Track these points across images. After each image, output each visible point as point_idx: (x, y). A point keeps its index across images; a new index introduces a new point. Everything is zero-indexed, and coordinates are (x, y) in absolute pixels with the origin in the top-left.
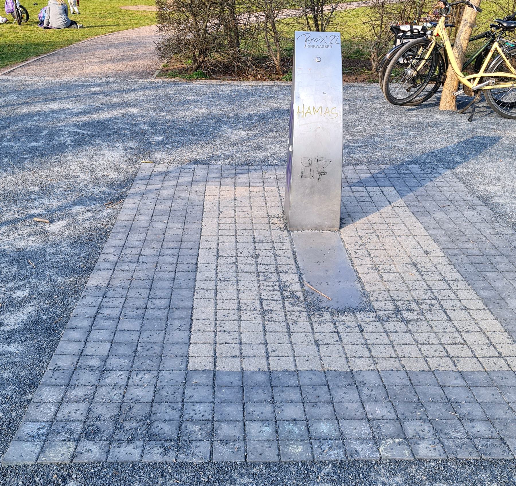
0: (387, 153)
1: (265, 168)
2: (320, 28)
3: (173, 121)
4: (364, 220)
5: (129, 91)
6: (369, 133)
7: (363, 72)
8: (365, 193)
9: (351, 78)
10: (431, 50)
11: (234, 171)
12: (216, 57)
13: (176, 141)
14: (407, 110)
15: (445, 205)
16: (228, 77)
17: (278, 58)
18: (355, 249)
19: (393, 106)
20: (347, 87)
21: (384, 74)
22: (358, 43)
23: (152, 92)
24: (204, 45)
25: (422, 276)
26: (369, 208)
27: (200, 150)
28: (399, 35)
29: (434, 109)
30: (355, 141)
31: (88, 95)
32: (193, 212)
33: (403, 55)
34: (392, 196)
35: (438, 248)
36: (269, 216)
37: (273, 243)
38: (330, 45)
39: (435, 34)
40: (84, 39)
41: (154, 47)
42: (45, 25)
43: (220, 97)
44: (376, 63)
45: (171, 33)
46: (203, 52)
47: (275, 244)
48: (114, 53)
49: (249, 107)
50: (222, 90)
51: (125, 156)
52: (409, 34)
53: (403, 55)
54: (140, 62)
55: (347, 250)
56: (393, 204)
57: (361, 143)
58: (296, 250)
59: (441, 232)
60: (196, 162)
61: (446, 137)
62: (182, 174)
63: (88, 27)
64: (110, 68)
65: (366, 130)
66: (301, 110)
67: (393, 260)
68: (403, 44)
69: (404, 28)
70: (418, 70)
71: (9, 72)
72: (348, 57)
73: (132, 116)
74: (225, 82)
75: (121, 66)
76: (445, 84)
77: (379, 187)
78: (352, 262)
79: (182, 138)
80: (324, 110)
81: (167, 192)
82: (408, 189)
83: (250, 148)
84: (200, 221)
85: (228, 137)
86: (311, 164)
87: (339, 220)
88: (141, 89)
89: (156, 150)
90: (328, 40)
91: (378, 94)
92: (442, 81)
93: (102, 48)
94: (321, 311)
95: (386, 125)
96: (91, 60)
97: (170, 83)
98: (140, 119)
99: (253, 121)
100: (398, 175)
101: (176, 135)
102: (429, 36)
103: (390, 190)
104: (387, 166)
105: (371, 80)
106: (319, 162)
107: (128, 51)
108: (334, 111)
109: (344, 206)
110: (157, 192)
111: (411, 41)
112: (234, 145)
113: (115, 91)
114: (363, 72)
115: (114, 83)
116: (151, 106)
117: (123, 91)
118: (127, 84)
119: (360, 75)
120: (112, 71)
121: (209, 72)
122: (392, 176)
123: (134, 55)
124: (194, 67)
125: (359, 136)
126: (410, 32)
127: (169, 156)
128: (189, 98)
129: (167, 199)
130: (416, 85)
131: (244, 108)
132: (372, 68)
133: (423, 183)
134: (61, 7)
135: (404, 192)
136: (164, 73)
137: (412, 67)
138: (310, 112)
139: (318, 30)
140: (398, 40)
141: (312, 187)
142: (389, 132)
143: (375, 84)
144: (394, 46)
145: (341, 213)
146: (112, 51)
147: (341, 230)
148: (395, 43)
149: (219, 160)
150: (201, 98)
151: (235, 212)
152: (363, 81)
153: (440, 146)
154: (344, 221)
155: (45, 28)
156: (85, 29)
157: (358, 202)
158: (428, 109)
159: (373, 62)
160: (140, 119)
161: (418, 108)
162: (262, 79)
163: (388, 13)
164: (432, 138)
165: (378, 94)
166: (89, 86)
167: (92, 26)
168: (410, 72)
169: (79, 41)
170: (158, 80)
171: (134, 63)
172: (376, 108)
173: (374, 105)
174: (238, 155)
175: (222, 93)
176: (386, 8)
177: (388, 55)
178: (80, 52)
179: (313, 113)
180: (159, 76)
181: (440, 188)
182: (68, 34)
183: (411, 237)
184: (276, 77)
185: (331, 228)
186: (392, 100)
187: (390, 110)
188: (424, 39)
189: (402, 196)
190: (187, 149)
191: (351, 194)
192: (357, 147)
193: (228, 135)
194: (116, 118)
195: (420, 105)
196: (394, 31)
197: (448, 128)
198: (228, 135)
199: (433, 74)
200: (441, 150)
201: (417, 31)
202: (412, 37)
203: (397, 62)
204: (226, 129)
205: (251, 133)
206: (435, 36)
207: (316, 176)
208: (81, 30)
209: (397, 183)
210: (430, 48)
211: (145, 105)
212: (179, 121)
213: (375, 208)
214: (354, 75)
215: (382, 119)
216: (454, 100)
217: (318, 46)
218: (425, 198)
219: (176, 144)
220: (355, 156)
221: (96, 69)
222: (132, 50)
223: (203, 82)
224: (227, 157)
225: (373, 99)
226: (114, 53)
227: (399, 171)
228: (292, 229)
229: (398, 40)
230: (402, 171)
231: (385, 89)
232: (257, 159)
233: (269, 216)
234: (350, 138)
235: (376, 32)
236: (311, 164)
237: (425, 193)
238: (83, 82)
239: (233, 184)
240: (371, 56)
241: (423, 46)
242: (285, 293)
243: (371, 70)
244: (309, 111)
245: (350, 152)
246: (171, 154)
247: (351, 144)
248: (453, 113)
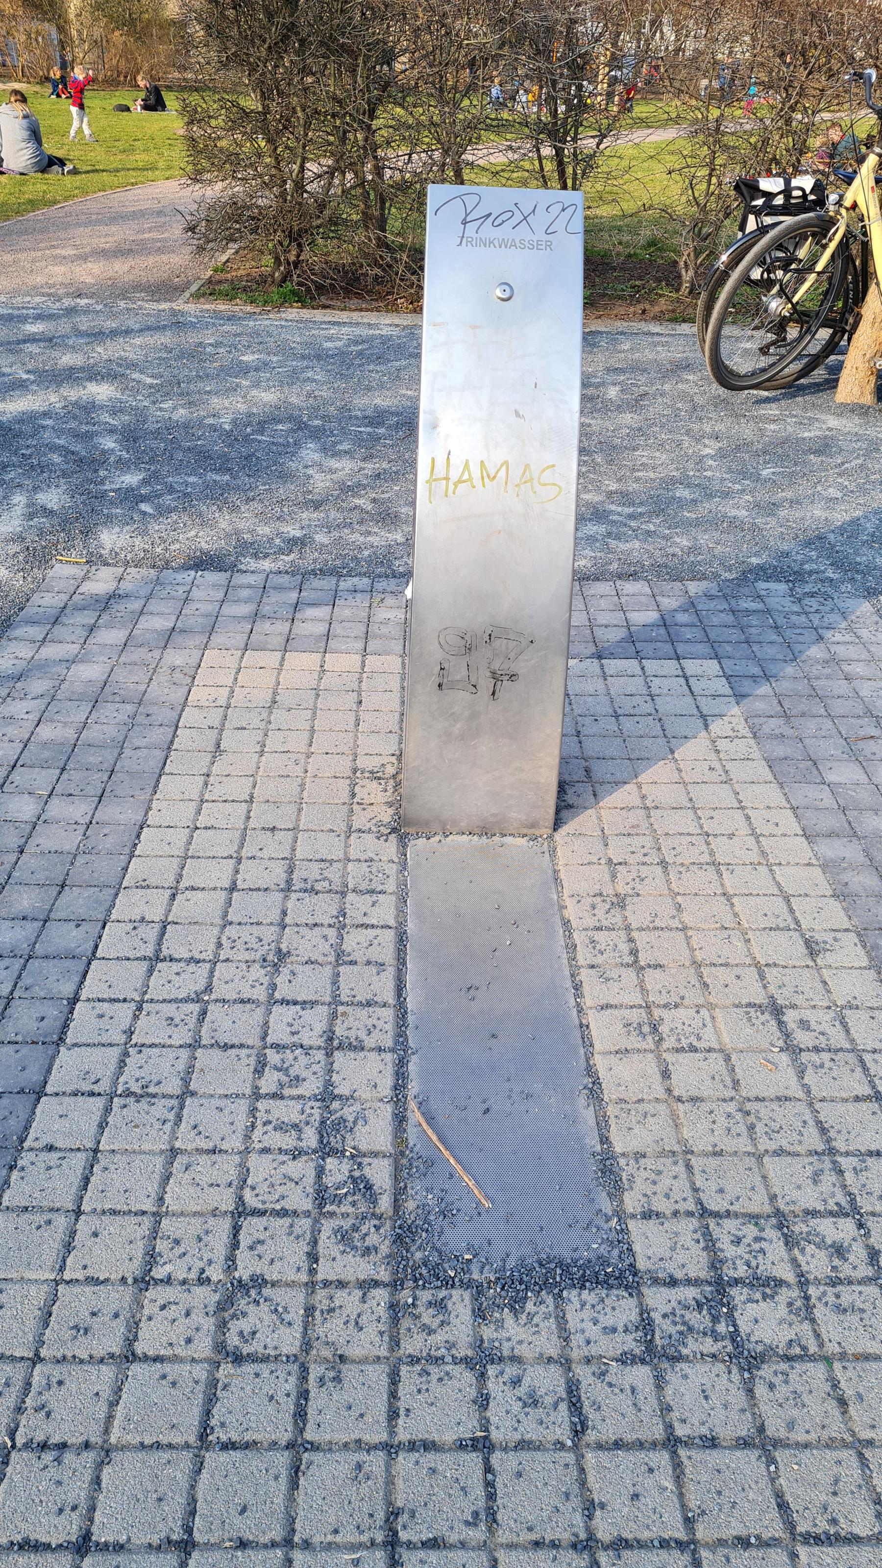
0: (704, 539)
1: (381, 585)
2: (569, 182)
3: (186, 426)
4: (625, 795)
5: (114, 333)
6: (662, 473)
7: (661, 296)
8: (636, 685)
9: (632, 309)
10: (833, 246)
11: (294, 595)
12: (325, 252)
13: (171, 490)
14: (757, 402)
15: (862, 733)
16: (354, 303)
18: (591, 922)
19: (722, 391)
20: (622, 333)
21: (709, 308)
22: (656, 222)
23: (166, 339)
24: (298, 222)
25: (801, 1073)
26: (646, 742)
27: (224, 521)
28: (754, 203)
29: (820, 398)
30: (625, 498)
31: (9, 343)
32: (139, 753)
33: (760, 261)
34: (714, 696)
35: (847, 925)
36: (355, 771)
37: (343, 894)
39: (848, 203)
40: (66, 199)
43: (321, 356)
44: (691, 273)
45: (216, 190)
46: (296, 237)
47: (351, 897)
48: (118, 234)
49: (382, 386)
50: (330, 339)
51: (19, 538)
52: (779, 201)
53: (760, 261)
54: (165, 258)
55: (566, 923)
56: (716, 727)
57: (641, 504)
58: (411, 927)
59: (852, 852)
60: (202, 562)
61: (852, 487)
62: (152, 606)
63: (88, 172)
64: (90, 273)
65: (654, 463)
66: (440, 471)
67: (706, 985)
68: (763, 230)
69: (768, 184)
70: (795, 300)
72: (630, 256)
73: (89, 408)
74: (344, 316)
75: (120, 267)
76: (855, 336)
77: (678, 659)
78: (578, 987)
79: (192, 479)
81: (90, 673)
82: (756, 671)
83: (355, 516)
84: (149, 790)
85: (309, 477)
86: (469, 649)
87: (554, 788)
88: (141, 330)
89: (109, 520)
90: (539, 221)
91: (691, 355)
92: (848, 328)
93: (99, 222)
94: (438, 1276)
95: (705, 446)
96: (58, 251)
97: (216, 314)
98: (105, 417)
99: (382, 431)
100: (729, 619)
101: (177, 471)
102: (832, 208)
103: (705, 670)
104: (704, 584)
105: (678, 318)
106: (497, 643)
107: (150, 230)
108: (547, 477)
109: (574, 733)
110: (61, 669)
111: (788, 220)
112: (317, 505)
113: (79, 333)
114: (661, 296)
115: (86, 311)
116: (149, 381)
117: (98, 336)
118: (114, 316)
119: (653, 303)
120: (93, 281)
121: (308, 290)
122: (715, 620)
123: (159, 240)
124: (277, 274)
125: (637, 480)
126: (781, 196)
127: (138, 541)
128: (245, 358)
129: (80, 698)
130: (785, 339)
131: (369, 389)
132: (680, 284)
133: (797, 648)
134: (25, 122)
136: (212, 289)
137: (782, 292)
138: (470, 479)
139: (564, 187)
140: (751, 218)
141: (474, 716)
142: (714, 471)
143: (685, 328)
144: (740, 235)
145: (564, 761)
146: (114, 228)
147: (559, 836)
148: (742, 227)
149: (266, 556)
150: (275, 359)
151: (262, 753)
152: (658, 318)
153: (840, 517)
154: (570, 798)
156: (79, 177)
157: (617, 716)
158: (807, 398)
159: (683, 272)
160: (105, 417)
161: (785, 396)
163: (726, 148)
164: (819, 488)
165: (691, 355)
166: (23, 319)
167: (96, 171)
168: (776, 305)
169: (55, 202)
170: (191, 307)
171: (151, 260)
172: (683, 396)
173: (680, 386)
174: (321, 538)
175: (329, 345)
176: (724, 134)
177: (724, 258)
178: (43, 230)
179: (477, 482)
180: (197, 296)
181: (846, 668)
182: (38, 185)
183: (763, 869)
185: (529, 831)
186: (725, 376)
187: (717, 403)
188: (818, 217)
189: (740, 697)
190: (190, 516)
191: (600, 685)
192: (631, 517)
193: (310, 471)
194: (46, 415)
195: (792, 388)
196: (742, 194)
197: (858, 457)
198: (310, 471)
199: (831, 309)
200: (842, 530)
201: (800, 193)
202: (786, 210)
203: (746, 280)
204: (310, 453)
205: (370, 467)
206: (847, 209)
207: (486, 684)
208: (68, 179)
209: (728, 648)
210: (830, 240)
211: (136, 375)
212: (201, 425)
213: (662, 741)
214: (639, 302)
215: (696, 427)
216: (873, 379)
217: (504, 244)
218: (803, 707)
219: (168, 500)
220: (623, 546)
221: (59, 273)
222: (158, 228)
223: (293, 313)
224: (293, 543)
225: (680, 367)
226: (118, 234)
228: (412, 830)
229: (751, 218)
231: (711, 350)
232: (366, 553)
233: (355, 771)
234: (614, 487)
235: (697, 195)
236: (469, 649)
237: (802, 687)
238: (13, 308)
239: (280, 641)
240: (680, 255)
241: (814, 235)
242: (337, 1171)
243: (678, 290)
244: (466, 476)
245: (609, 534)
246: (145, 532)
247: (613, 507)
248: (866, 413)
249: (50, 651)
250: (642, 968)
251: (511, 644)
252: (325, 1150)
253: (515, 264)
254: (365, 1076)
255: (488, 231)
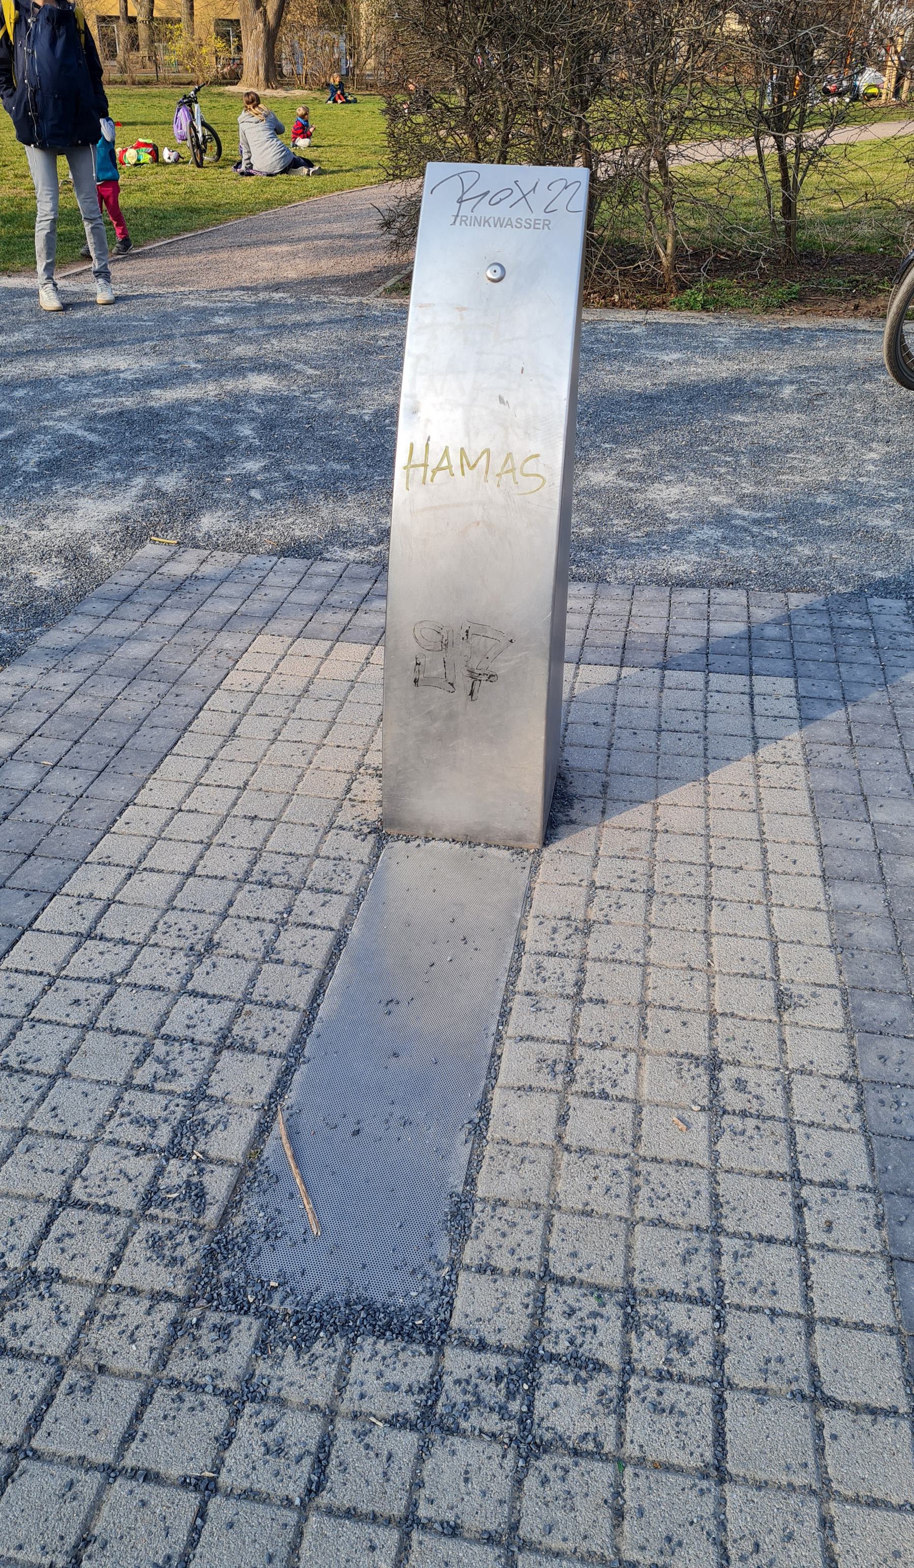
4: (639, 815)
17: (669, 251)
26: (680, 761)
38: (544, 216)
41: (377, 219)
42: (243, 168)
66: (418, 457)
67: (645, 1028)
71: (78, 274)
80: (498, 462)
86: (445, 645)
90: (538, 200)
95: (871, 450)
103: (777, 689)
106: (474, 641)
114: (880, 291)
135: (818, 705)
138: (449, 467)
155: (242, 174)
162: (622, 305)
179: (457, 471)
182: (280, 186)
184: (658, 298)
192: (756, 522)
207: (463, 683)
209: (812, 666)
217: (500, 223)
227: (836, 618)
230: (847, 621)
236: (445, 645)
244: (445, 464)
249: (112, 628)
250: (583, 1002)
251: (490, 642)
252: (174, 1150)
253: (507, 244)
254: (244, 1080)
255: (484, 209)
